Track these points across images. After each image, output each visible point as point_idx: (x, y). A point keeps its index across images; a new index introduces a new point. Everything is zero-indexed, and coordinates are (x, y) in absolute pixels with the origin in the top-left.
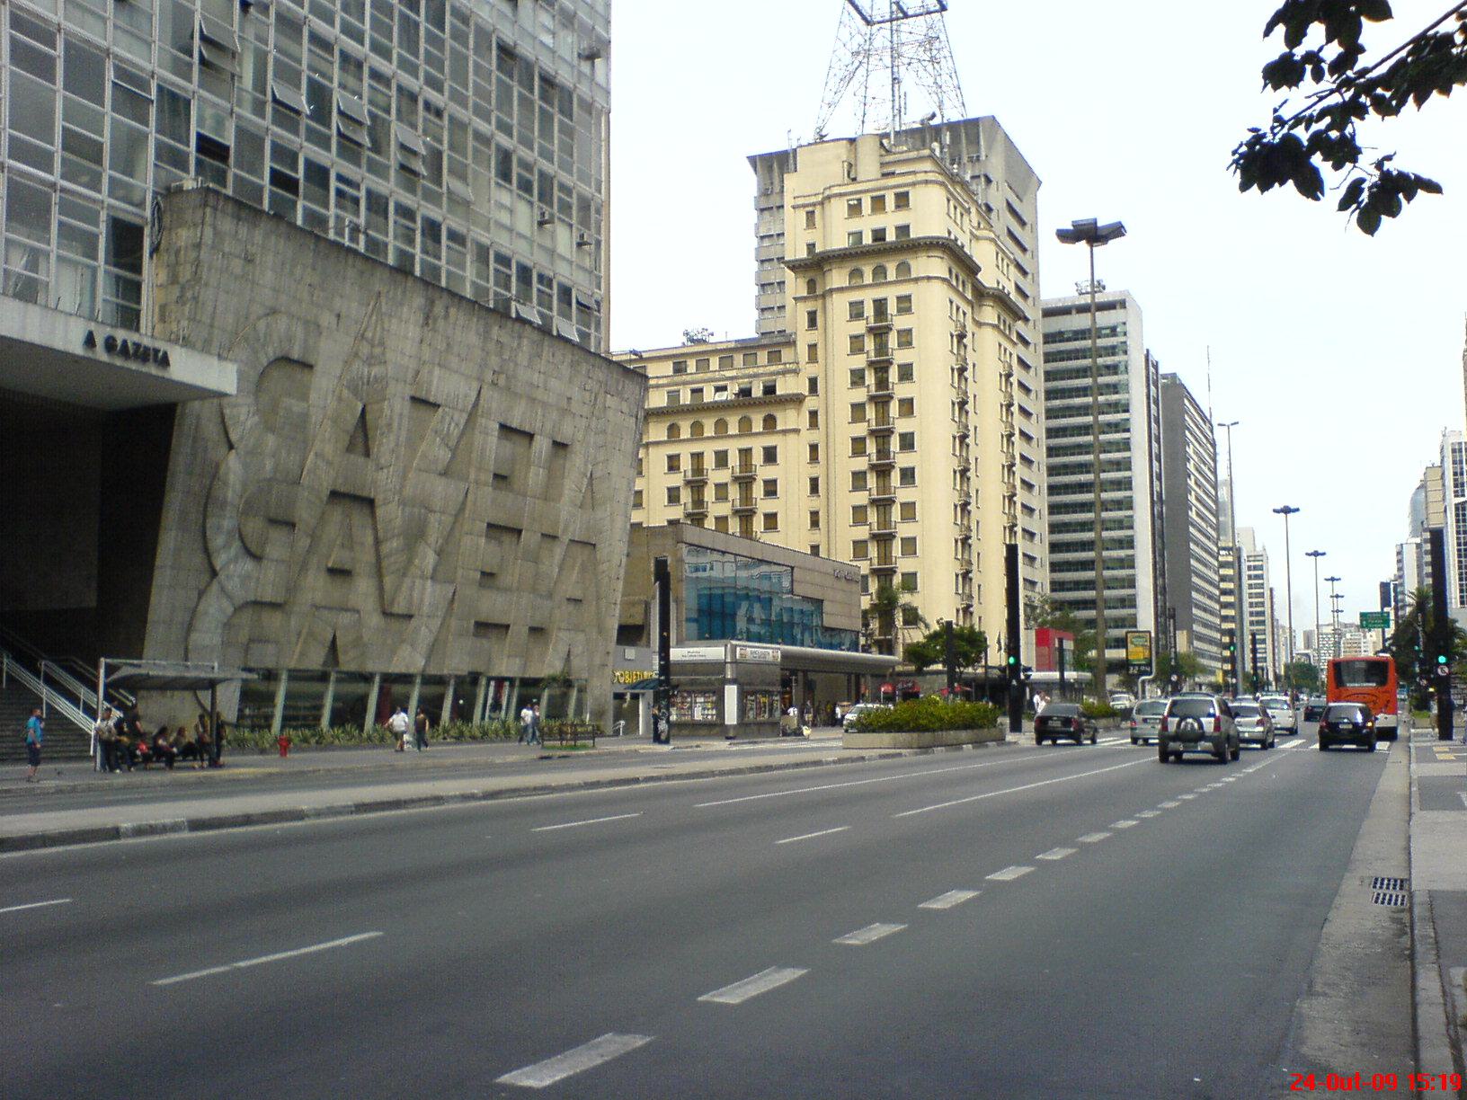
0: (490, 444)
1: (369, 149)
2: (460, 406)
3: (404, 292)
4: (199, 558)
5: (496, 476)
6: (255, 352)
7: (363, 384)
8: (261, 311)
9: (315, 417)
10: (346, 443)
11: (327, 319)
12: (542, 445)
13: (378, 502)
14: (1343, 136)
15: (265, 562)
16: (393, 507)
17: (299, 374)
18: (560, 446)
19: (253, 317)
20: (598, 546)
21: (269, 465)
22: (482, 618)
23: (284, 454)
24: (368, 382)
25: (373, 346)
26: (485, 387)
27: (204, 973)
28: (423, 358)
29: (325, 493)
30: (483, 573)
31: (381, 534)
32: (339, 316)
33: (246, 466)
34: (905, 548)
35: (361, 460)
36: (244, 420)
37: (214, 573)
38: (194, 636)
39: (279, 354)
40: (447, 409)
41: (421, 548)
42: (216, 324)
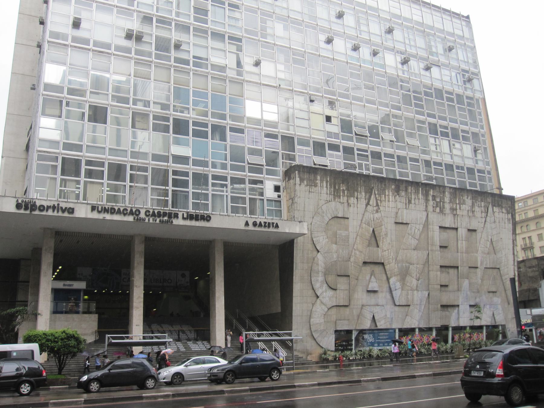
0: (437, 236)
1: (369, 136)
2: (418, 223)
3: (385, 185)
4: (311, 291)
5: (441, 247)
8: (324, 202)
9: (352, 236)
10: (367, 244)
12: (462, 232)
13: (385, 264)
16: (392, 264)
18: (472, 231)
19: (320, 205)
20: (500, 269)
22: (444, 304)
23: (341, 251)
24: (374, 220)
26: (429, 213)
28: (398, 207)
29: (361, 264)
30: (441, 286)
31: (389, 276)
33: (324, 257)
34: (59, 385)
35: (376, 249)
36: (322, 241)
37: (318, 297)
38: (312, 320)
40: (412, 225)
41: (408, 278)
42: (306, 210)
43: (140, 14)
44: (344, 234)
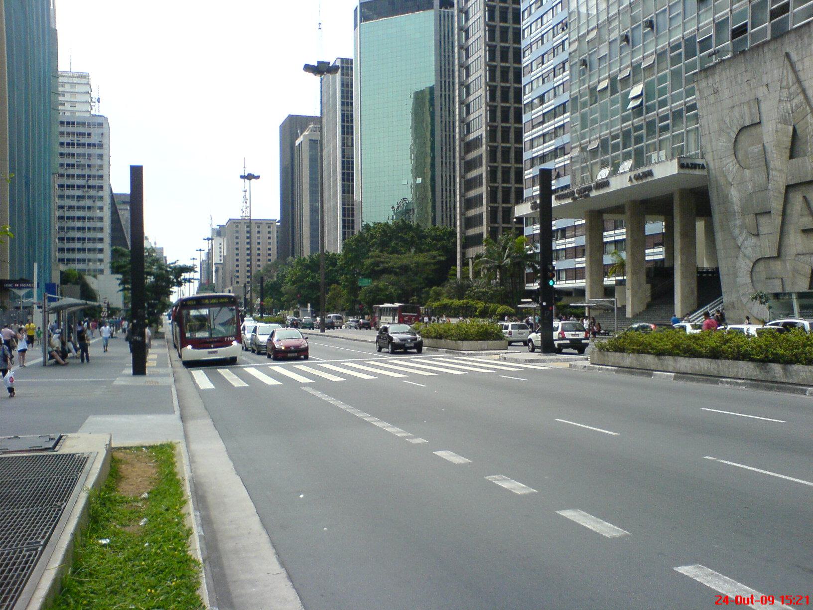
6: (728, 133)
7: (789, 114)
11: (761, 92)
14: (132, 322)
15: (761, 236)
17: (754, 131)
21: (750, 186)
25: (789, 89)
27: (580, 425)
32: (767, 85)
33: (739, 191)
39: (739, 128)
43: (427, 104)
44: (756, 150)
